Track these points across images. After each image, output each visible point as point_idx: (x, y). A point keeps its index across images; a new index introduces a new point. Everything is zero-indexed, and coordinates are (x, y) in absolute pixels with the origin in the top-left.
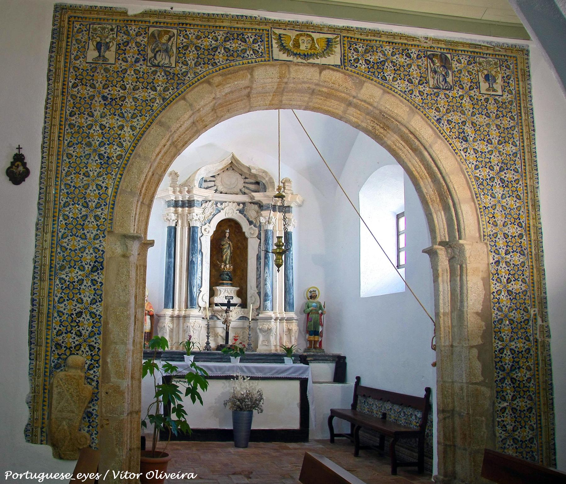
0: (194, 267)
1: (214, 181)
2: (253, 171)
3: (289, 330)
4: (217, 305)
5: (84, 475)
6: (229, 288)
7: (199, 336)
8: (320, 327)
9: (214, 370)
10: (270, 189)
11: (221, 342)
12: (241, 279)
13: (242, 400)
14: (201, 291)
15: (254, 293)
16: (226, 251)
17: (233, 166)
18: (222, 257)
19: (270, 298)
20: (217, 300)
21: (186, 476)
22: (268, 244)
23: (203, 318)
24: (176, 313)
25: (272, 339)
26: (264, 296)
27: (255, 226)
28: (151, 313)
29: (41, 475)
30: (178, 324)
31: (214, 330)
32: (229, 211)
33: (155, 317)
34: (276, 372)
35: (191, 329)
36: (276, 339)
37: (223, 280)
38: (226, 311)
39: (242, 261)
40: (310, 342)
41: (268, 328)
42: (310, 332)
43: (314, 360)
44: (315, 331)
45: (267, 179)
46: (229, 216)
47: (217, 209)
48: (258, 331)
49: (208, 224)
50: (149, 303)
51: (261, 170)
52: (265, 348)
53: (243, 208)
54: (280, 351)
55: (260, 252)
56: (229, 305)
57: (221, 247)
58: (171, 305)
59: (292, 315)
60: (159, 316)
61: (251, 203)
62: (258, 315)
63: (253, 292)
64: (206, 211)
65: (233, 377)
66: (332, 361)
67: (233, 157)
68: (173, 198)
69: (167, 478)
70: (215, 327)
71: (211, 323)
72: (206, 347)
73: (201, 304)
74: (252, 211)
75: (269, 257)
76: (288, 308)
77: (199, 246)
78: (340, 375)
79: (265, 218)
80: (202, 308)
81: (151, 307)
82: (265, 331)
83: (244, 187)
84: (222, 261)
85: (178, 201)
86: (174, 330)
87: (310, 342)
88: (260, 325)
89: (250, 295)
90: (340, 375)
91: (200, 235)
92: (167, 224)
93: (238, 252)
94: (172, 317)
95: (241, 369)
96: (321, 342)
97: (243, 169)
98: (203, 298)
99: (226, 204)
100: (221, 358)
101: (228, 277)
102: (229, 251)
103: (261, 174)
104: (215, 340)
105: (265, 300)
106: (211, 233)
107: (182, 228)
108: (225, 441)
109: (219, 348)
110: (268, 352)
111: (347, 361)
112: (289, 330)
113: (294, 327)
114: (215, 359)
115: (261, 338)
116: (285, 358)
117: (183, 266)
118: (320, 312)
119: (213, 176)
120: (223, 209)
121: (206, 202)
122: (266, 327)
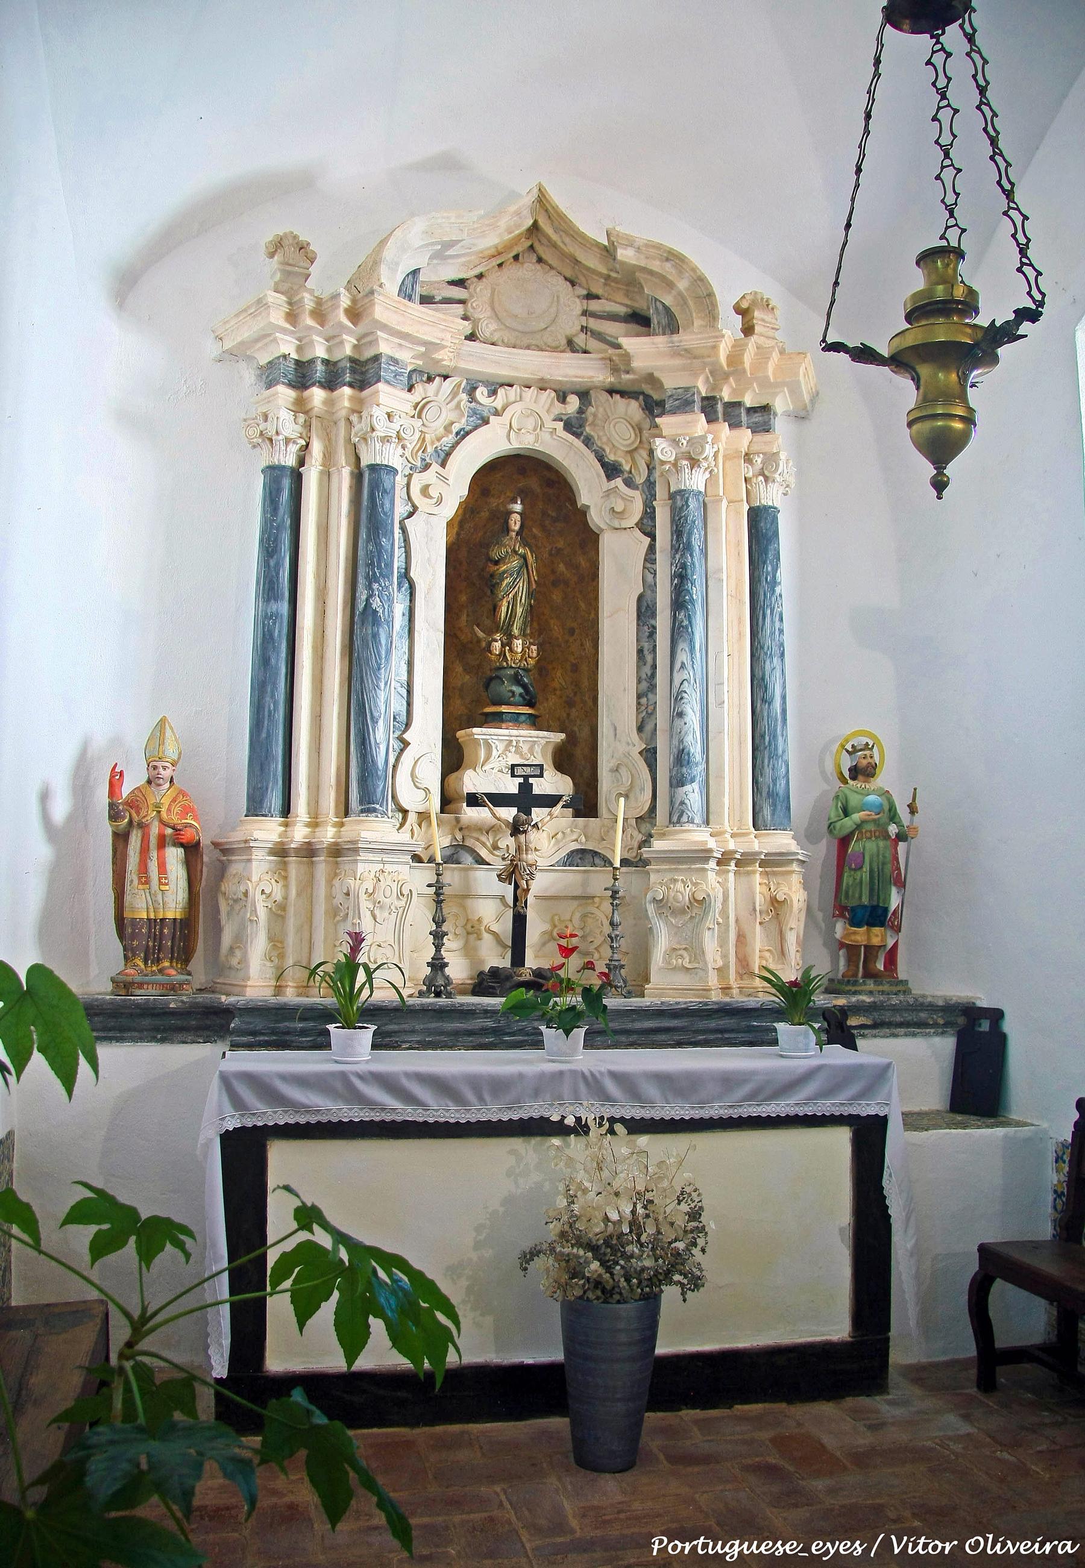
0: (375, 636)
1: (462, 302)
2: (625, 254)
3: (776, 905)
4: (473, 800)
6: (526, 734)
7: (399, 930)
8: (894, 890)
9: (470, 1096)
10: (698, 323)
11: (497, 959)
12: (570, 704)
13: (608, 1248)
14: (406, 744)
15: (628, 755)
16: (512, 585)
17: (541, 241)
18: (495, 608)
19: (698, 770)
20: (472, 781)
21: (1056, 1547)
22: (688, 547)
23: (417, 858)
24: (299, 834)
25: (710, 944)
26: (671, 767)
27: (629, 483)
28: (188, 835)
30: (308, 884)
31: (464, 907)
32: (523, 425)
33: (208, 856)
34: (751, 1097)
35: (365, 905)
36: (723, 942)
37: (500, 704)
38: (516, 829)
39: (572, 632)
40: (852, 950)
41: (694, 900)
42: (853, 910)
43: (875, 1026)
44: (874, 908)
45: (682, 285)
46: (525, 442)
47: (474, 412)
48: (651, 909)
49: (435, 467)
50: (182, 793)
51: (658, 247)
52: (681, 980)
53: (581, 411)
54: (765, 996)
55: (650, 587)
56: (525, 800)
57: (492, 568)
58: (275, 800)
59: (783, 841)
60: (225, 850)
61: (611, 392)
62: (646, 842)
63: (622, 748)
64: (430, 414)
65: (560, 1129)
66: (941, 1029)
67: (542, 201)
68: (288, 347)
70: (465, 896)
71: (451, 876)
72: (429, 982)
73: (410, 797)
74: (617, 423)
75: (692, 601)
76: (767, 812)
77: (399, 553)
78: (979, 1086)
79: (675, 442)
80: (412, 818)
81: (186, 810)
82: (683, 911)
83: (584, 329)
84: (495, 627)
85: (312, 361)
86: (291, 911)
87: (852, 950)
88: (659, 882)
89: (613, 763)
90: (979, 1086)
91: (401, 509)
92: (265, 458)
93: (557, 596)
94: (280, 851)
95: (593, 1085)
96: (892, 956)
97: (581, 256)
98: (416, 772)
99: (513, 393)
100: (495, 1031)
101: (518, 690)
102: (522, 587)
103: (655, 266)
104: (469, 951)
105: (678, 781)
106: (450, 509)
107: (326, 475)
108: (520, 1418)
109: (487, 982)
110: (691, 1000)
111: (1008, 1026)
112: (776, 905)
113: (794, 891)
114: (470, 1033)
115: (662, 941)
116: (781, 1026)
117: (329, 632)
118: (893, 829)
119: (460, 283)
120: (497, 413)
121: (430, 379)
122: (682, 891)
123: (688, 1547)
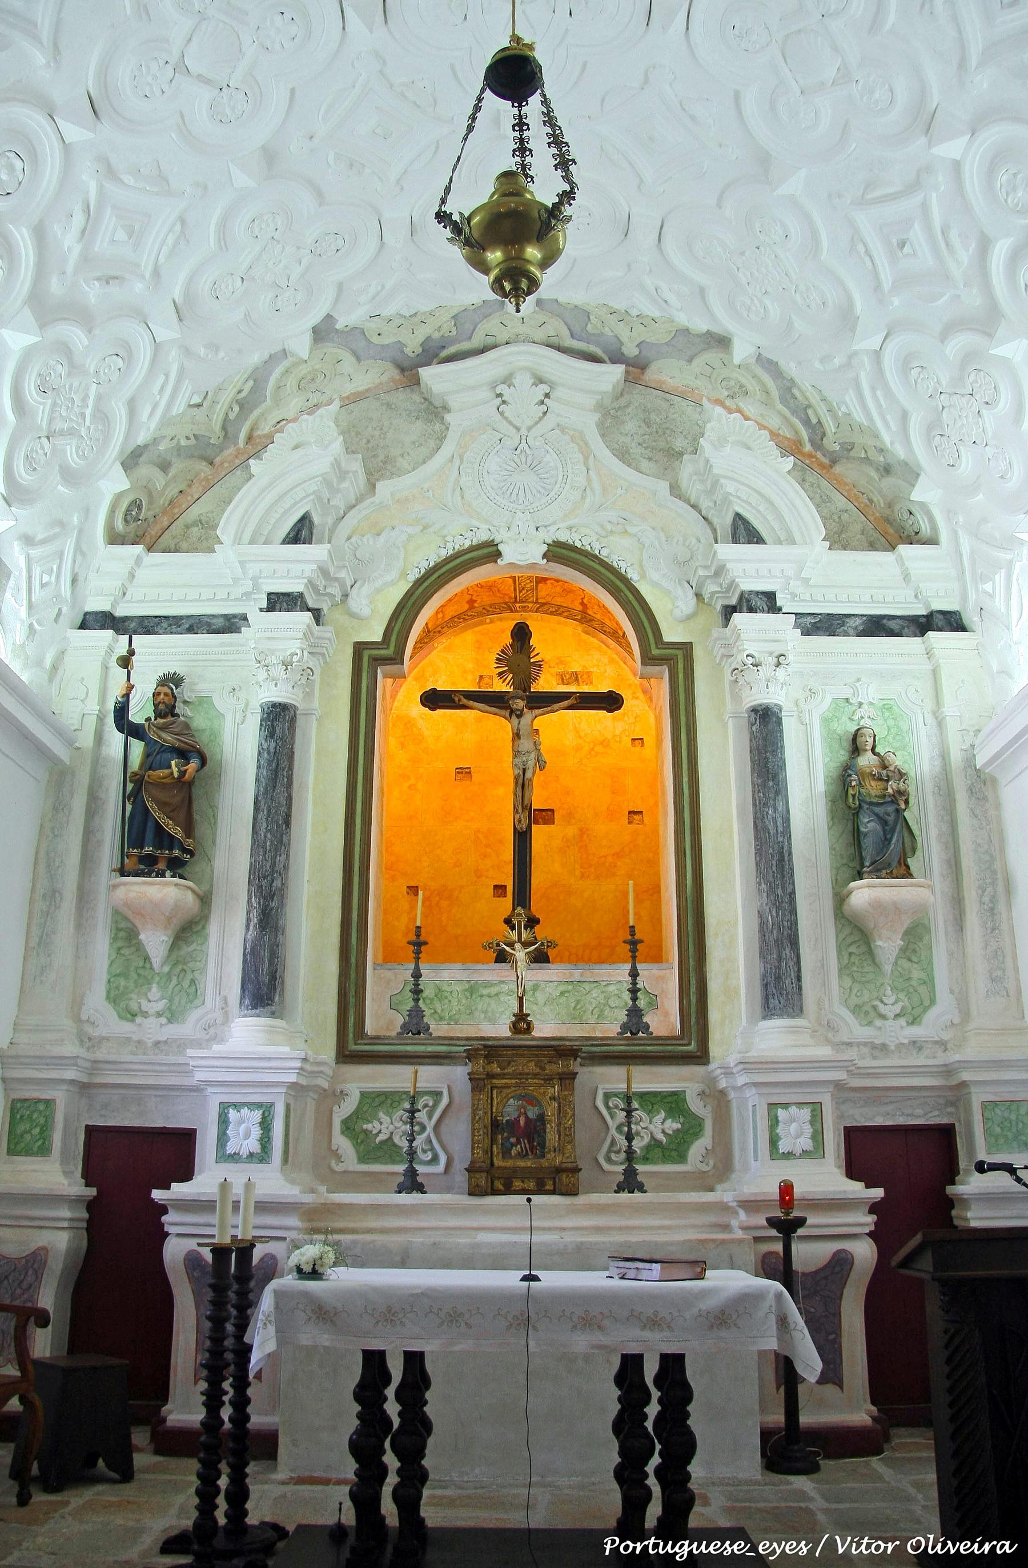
5: (775, 1545)
21: (994, 1547)
29: (682, 1545)
69: (952, 1552)
123: (639, 1547)
